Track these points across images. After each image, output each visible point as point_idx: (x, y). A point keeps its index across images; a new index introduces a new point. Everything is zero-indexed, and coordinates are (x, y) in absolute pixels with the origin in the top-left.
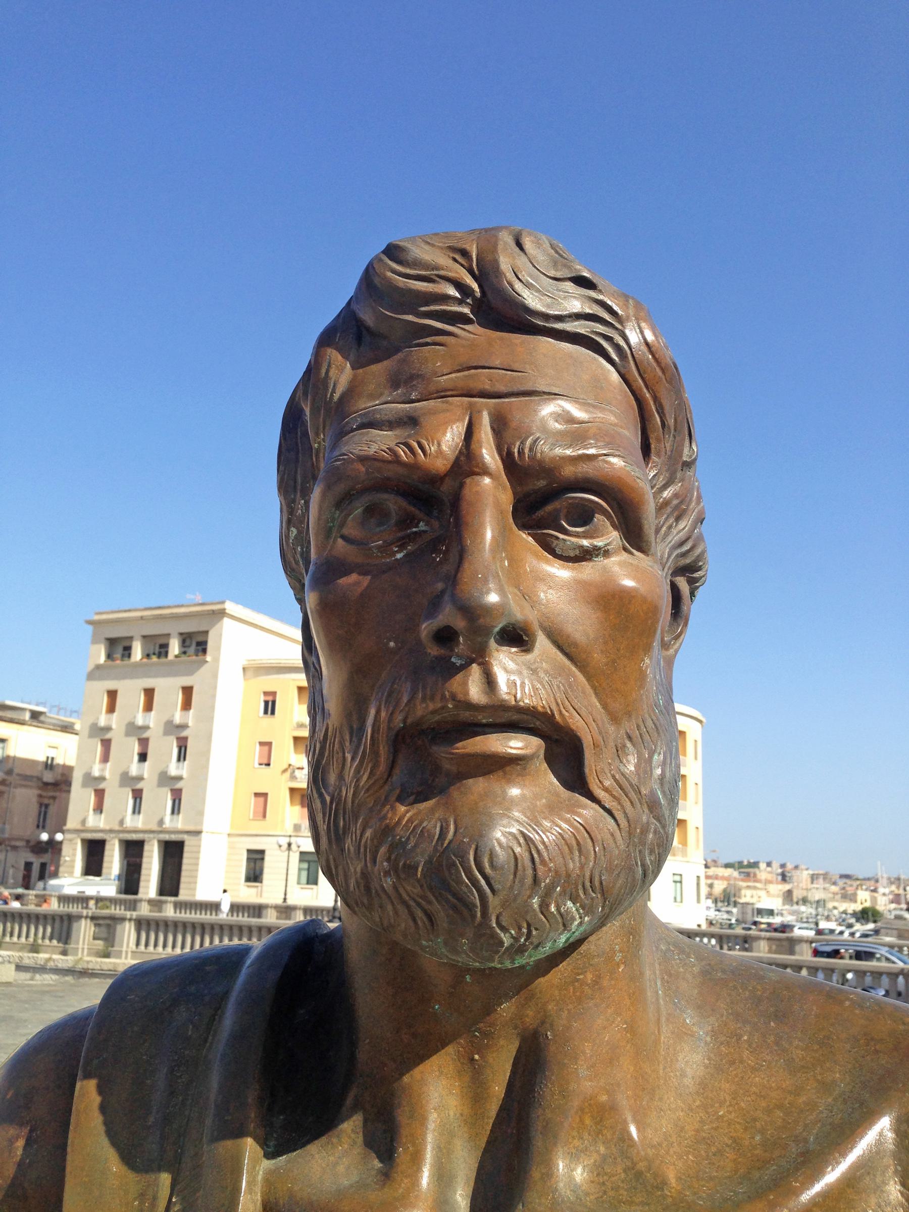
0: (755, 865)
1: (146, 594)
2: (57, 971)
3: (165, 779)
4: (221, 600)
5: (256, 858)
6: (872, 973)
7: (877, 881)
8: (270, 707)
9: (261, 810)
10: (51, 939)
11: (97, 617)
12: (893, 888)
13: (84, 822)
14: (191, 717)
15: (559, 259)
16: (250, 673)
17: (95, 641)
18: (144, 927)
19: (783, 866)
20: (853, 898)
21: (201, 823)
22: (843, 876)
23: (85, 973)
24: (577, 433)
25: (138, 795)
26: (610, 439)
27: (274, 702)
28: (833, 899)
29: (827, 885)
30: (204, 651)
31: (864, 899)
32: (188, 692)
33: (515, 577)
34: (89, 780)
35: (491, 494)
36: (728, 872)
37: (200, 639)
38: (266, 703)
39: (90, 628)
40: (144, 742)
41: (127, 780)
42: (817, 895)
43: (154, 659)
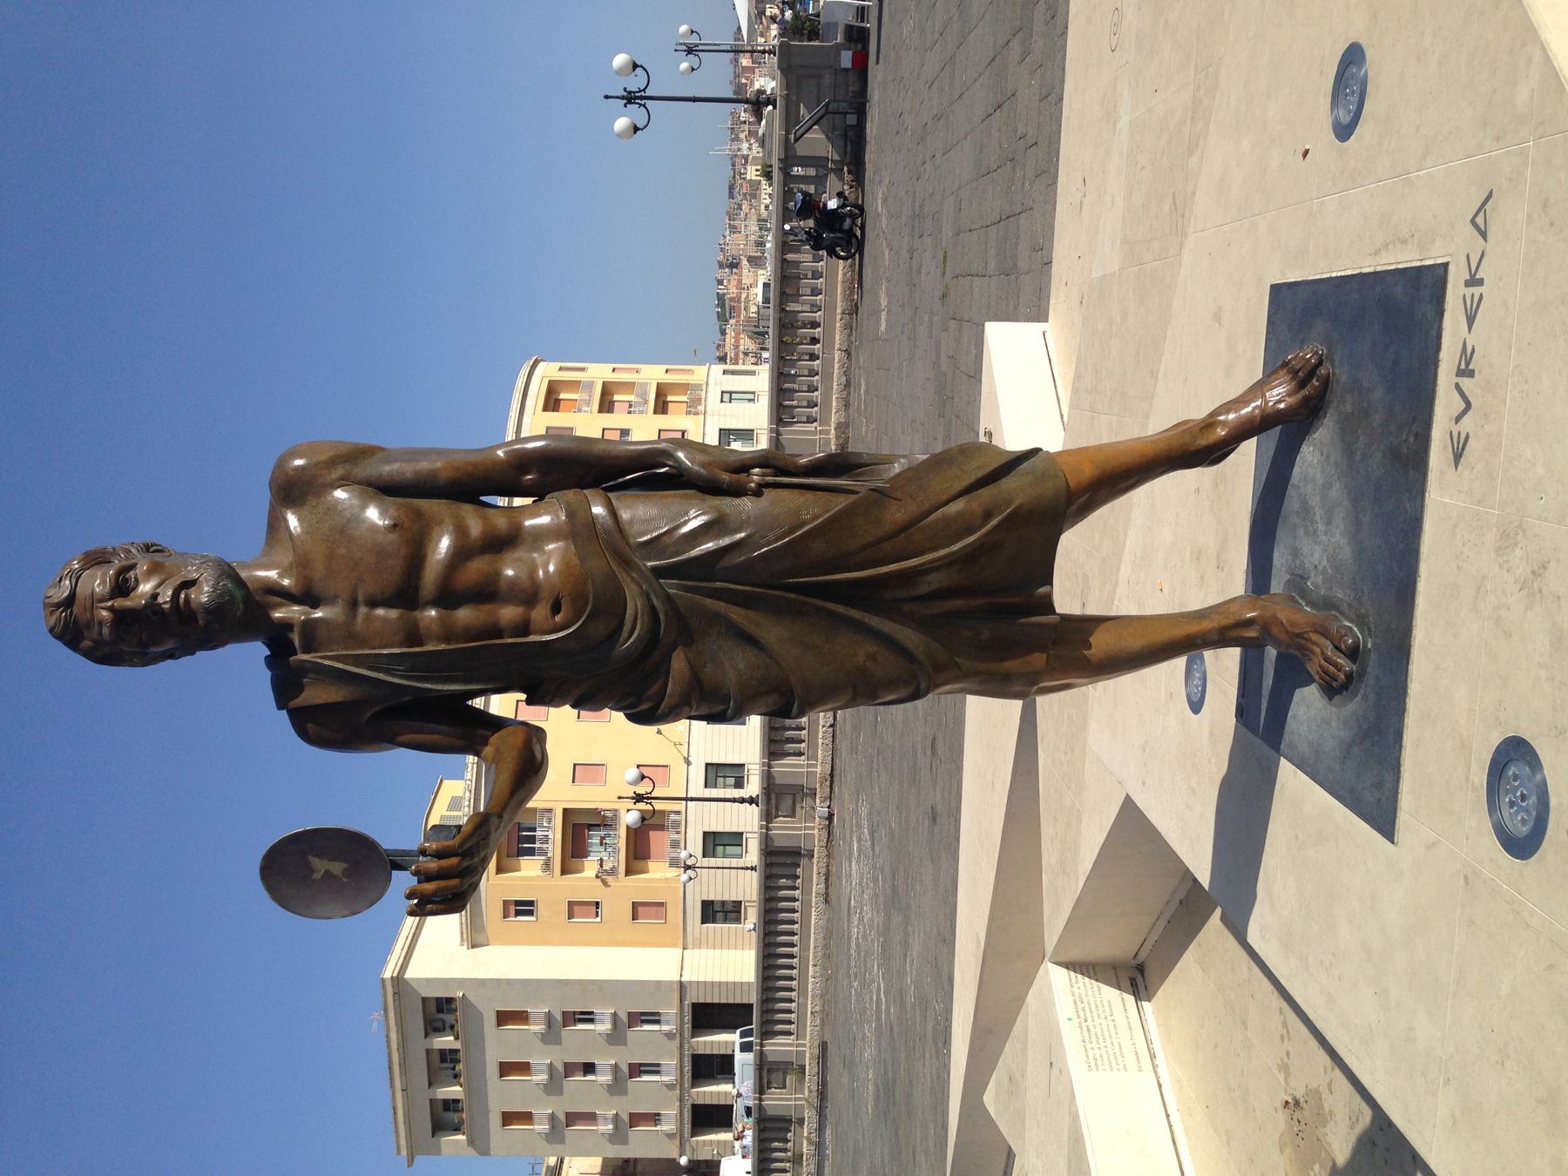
0: (721, 298)
1: (369, 1079)
2: (821, 1129)
3: (616, 1036)
4: (380, 985)
5: (713, 912)
8: (524, 908)
9: (654, 909)
10: (787, 1141)
11: (404, 1152)
13: (670, 1136)
14: (537, 1010)
15: (54, 586)
16: (480, 938)
17: (438, 1152)
18: (769, 1028)
19: (721, 266)
20: (755, 186)
21: (671, 982)
22: (731, 196)
23: (822, 1095)
24: (103, 582)
25: (637, 1070)
26: (104, 575)
27: (517, 903)
30: (450, 1000)
32: (504, 1018)
33: (141, 596)
34: (618, 1136)
35: (119, 603)
36: (730, 333)
37: (433, 1007)
38: (518, 913)
39: (418, 1158)
40: (570, 1069)
41: (617, 1087)
42: (754, 227)
43: (460, 1067)
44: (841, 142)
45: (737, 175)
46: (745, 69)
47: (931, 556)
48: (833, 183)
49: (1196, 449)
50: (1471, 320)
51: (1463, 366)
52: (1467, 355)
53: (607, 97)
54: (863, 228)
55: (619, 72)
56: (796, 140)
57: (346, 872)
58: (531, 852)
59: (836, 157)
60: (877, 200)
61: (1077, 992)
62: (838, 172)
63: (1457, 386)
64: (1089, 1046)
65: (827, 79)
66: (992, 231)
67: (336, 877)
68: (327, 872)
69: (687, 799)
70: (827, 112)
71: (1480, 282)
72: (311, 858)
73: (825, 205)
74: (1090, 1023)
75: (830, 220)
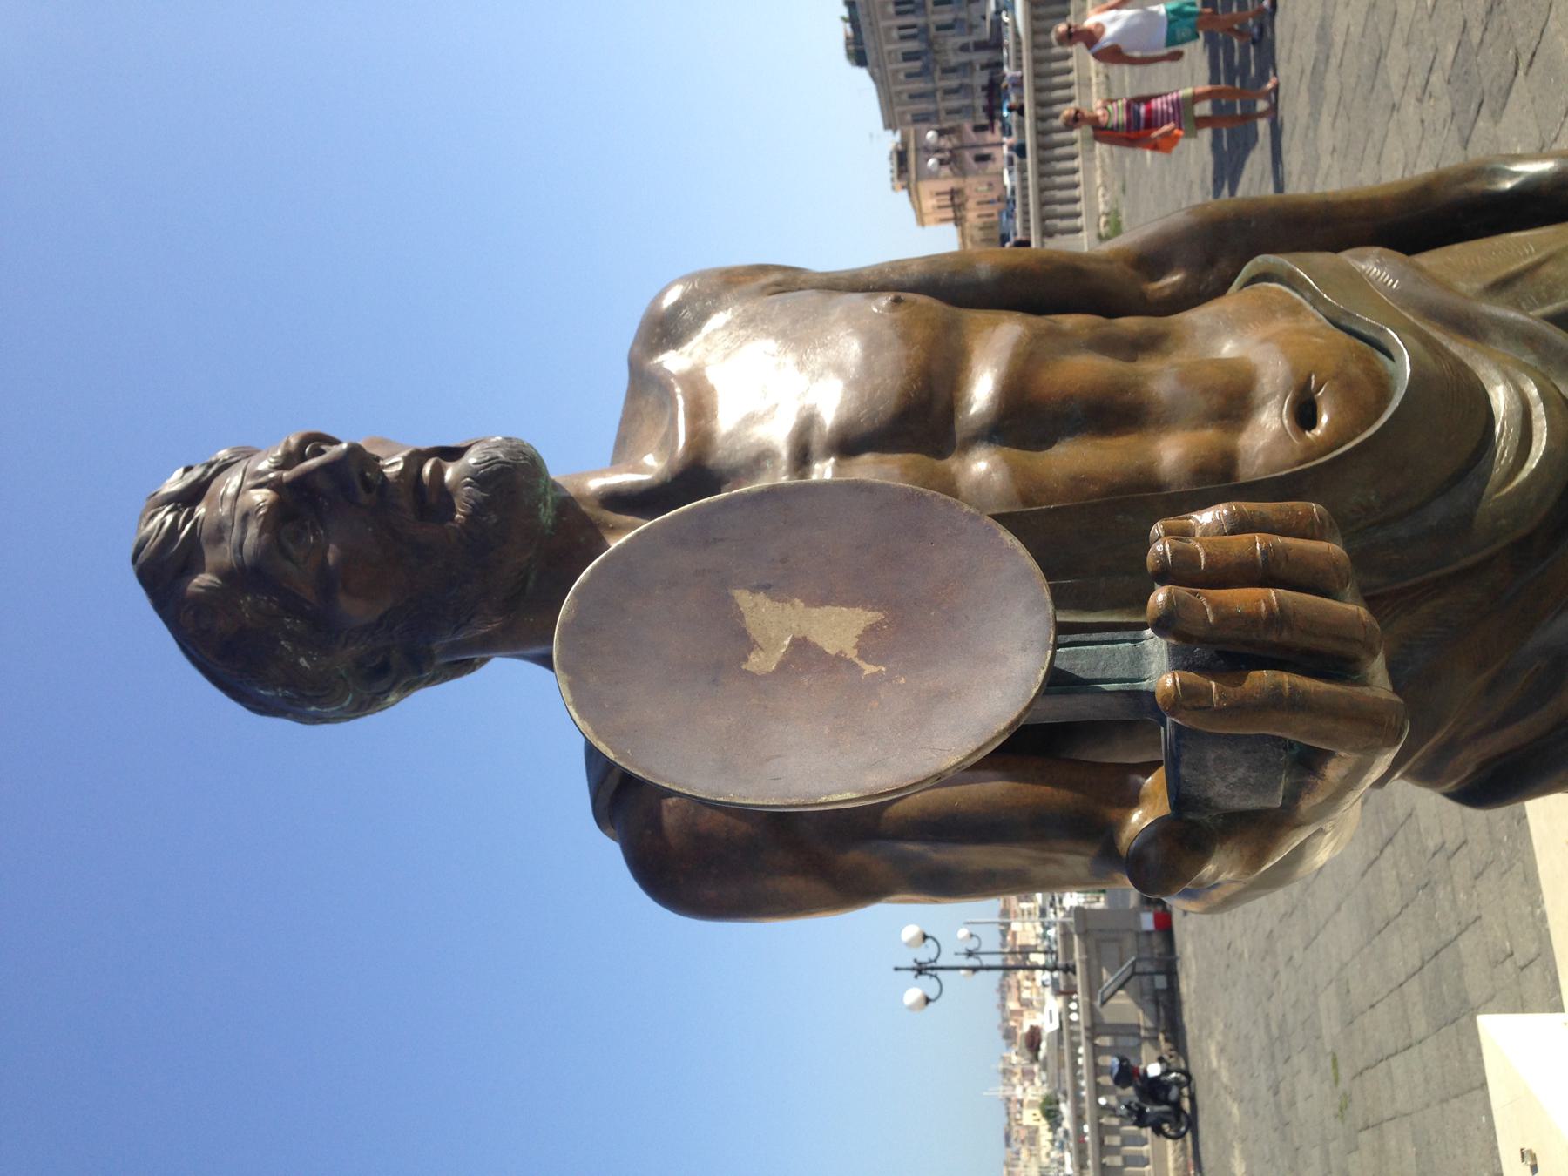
6: (1102, 1155)
7: (1009, 1099)
12: (1015, 1080)
22: (1008, 1144)
28: (1037, 1156)
29: (1021, 1163)
31: (1031, 1117)
44: (1152, 1008)
45: (1011, 1119)
46: (1014, 1013)
48: (1147, 1050)
53: (896, 969)
54: (1192, 1098)
55: (909, 944)
56: (1103, 1003)
57: (870, 643)
59: (1150, 1024)
60: (1211, 1058)
62: (1154, 1040)
65: (1129, 942)
66: (1414, 987)
67: (837, 663)
68: (801, 646)
70: (1134, 974)
72: (744, 598)
73: (1145, 1072)
75: (1153, 1089)
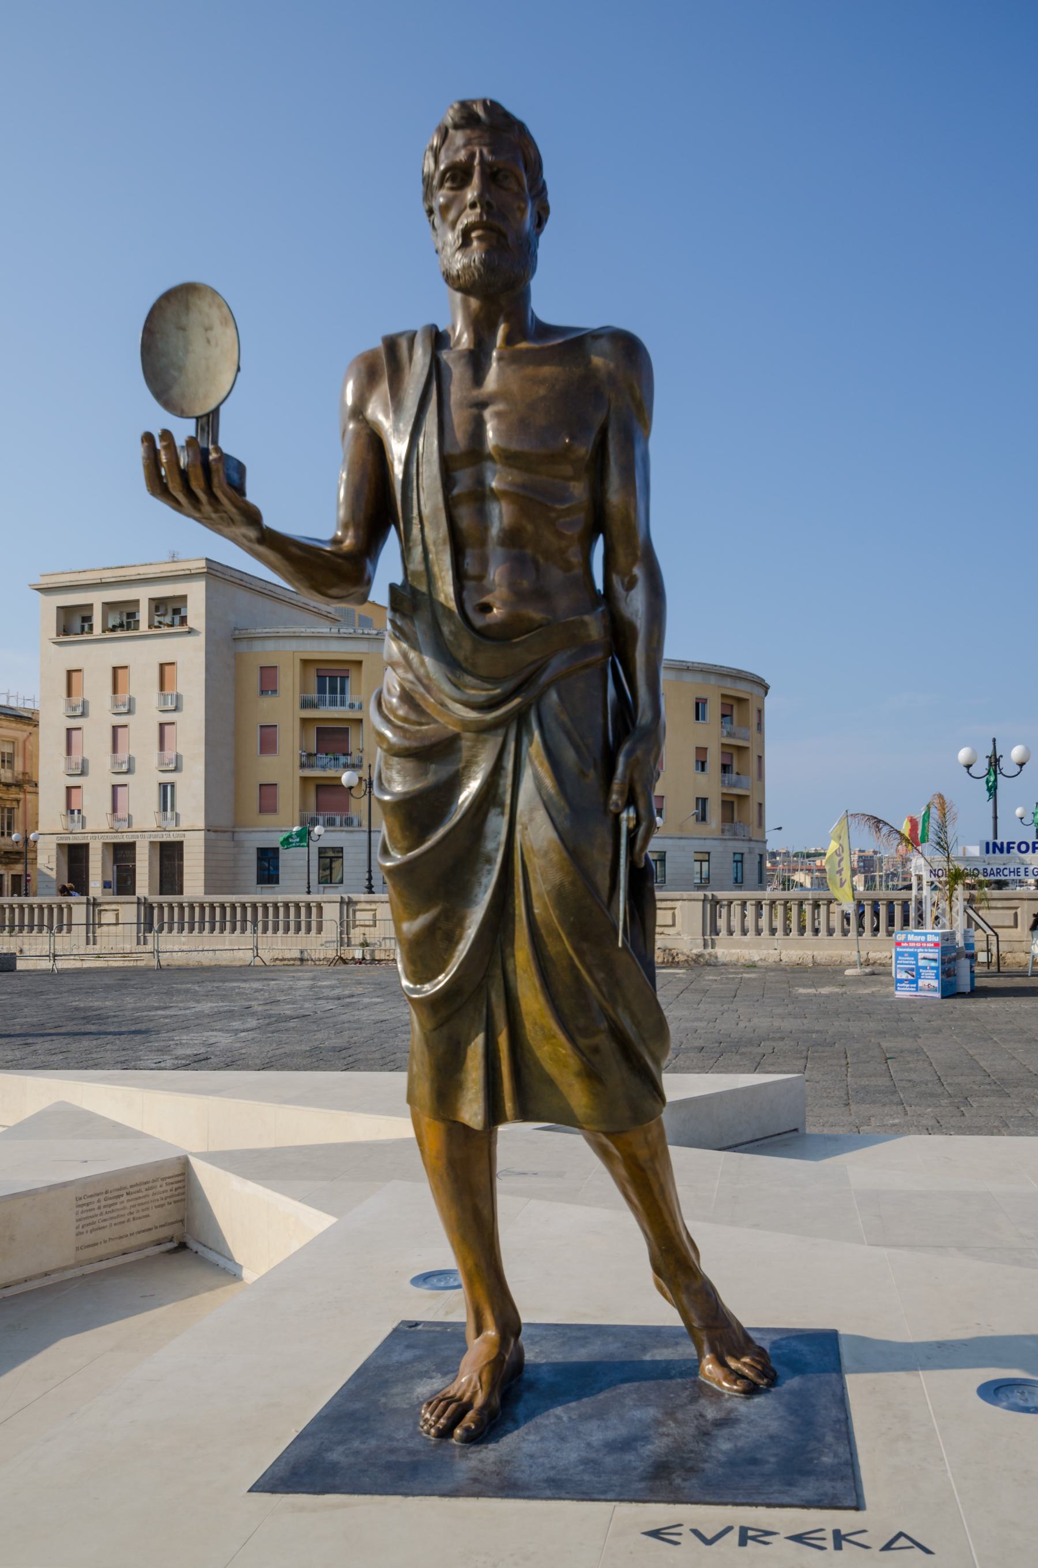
47: (974, 1554)
49: (675, 1262)
50: (798, 1538)
51: (750, 1533)
52: (763, 1536)
58: (321, 690)
61: (158, 1184)
63: (729, 1529)
64: (102, 1197)
69: (370, 832)
71: (838, 1547)
74: (125, 1198)
